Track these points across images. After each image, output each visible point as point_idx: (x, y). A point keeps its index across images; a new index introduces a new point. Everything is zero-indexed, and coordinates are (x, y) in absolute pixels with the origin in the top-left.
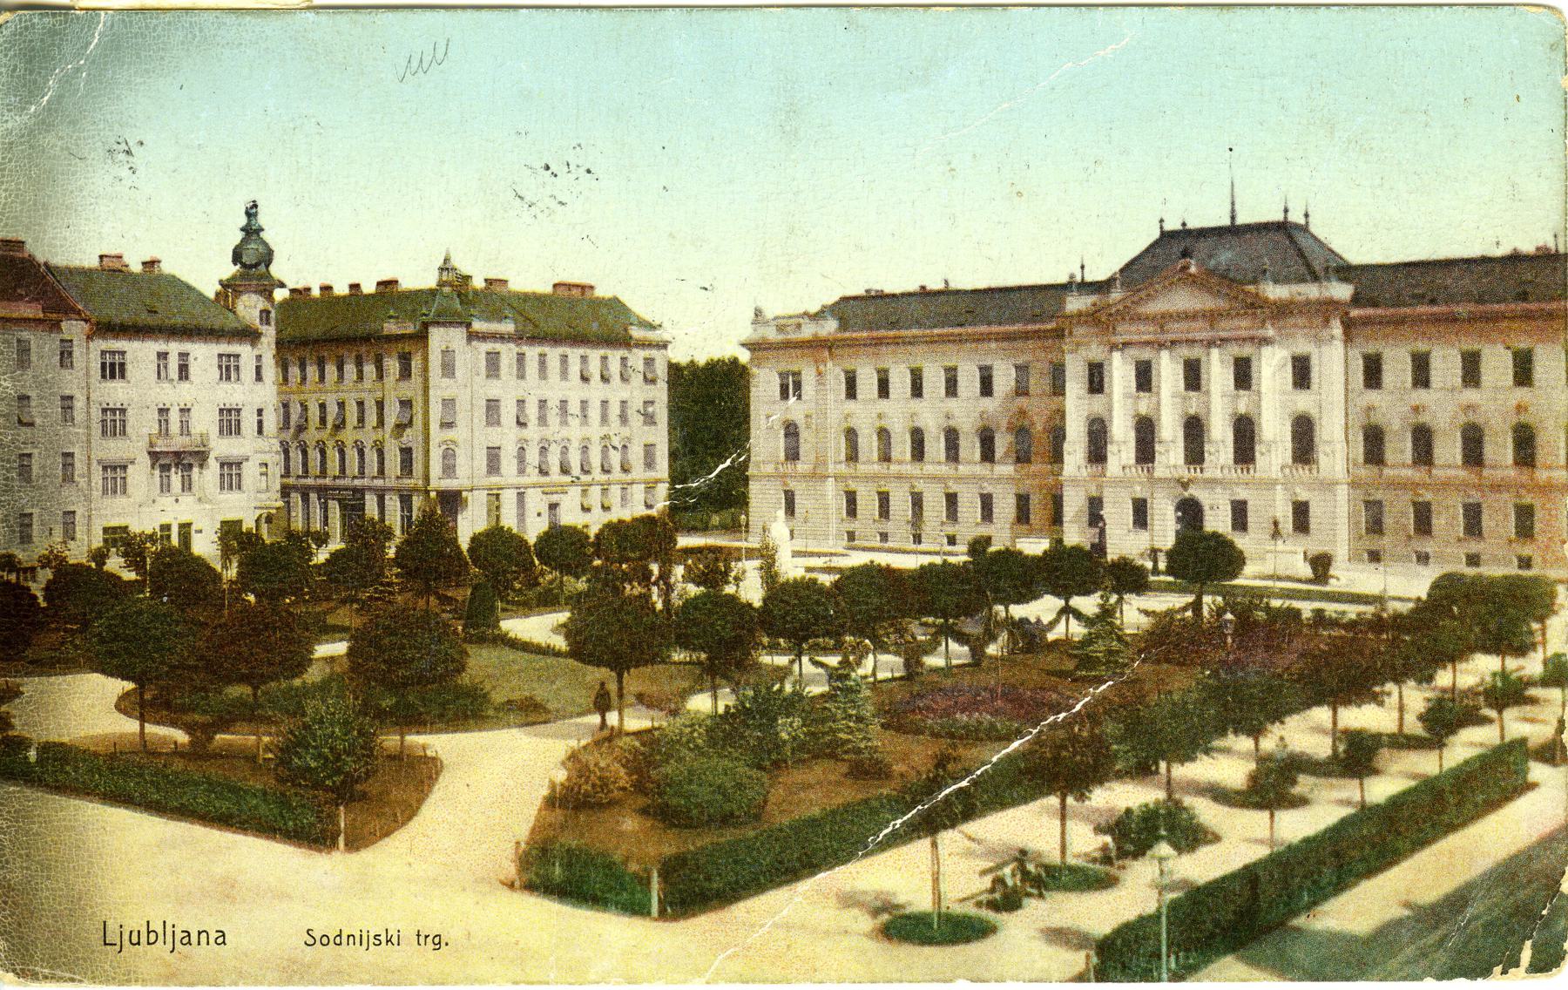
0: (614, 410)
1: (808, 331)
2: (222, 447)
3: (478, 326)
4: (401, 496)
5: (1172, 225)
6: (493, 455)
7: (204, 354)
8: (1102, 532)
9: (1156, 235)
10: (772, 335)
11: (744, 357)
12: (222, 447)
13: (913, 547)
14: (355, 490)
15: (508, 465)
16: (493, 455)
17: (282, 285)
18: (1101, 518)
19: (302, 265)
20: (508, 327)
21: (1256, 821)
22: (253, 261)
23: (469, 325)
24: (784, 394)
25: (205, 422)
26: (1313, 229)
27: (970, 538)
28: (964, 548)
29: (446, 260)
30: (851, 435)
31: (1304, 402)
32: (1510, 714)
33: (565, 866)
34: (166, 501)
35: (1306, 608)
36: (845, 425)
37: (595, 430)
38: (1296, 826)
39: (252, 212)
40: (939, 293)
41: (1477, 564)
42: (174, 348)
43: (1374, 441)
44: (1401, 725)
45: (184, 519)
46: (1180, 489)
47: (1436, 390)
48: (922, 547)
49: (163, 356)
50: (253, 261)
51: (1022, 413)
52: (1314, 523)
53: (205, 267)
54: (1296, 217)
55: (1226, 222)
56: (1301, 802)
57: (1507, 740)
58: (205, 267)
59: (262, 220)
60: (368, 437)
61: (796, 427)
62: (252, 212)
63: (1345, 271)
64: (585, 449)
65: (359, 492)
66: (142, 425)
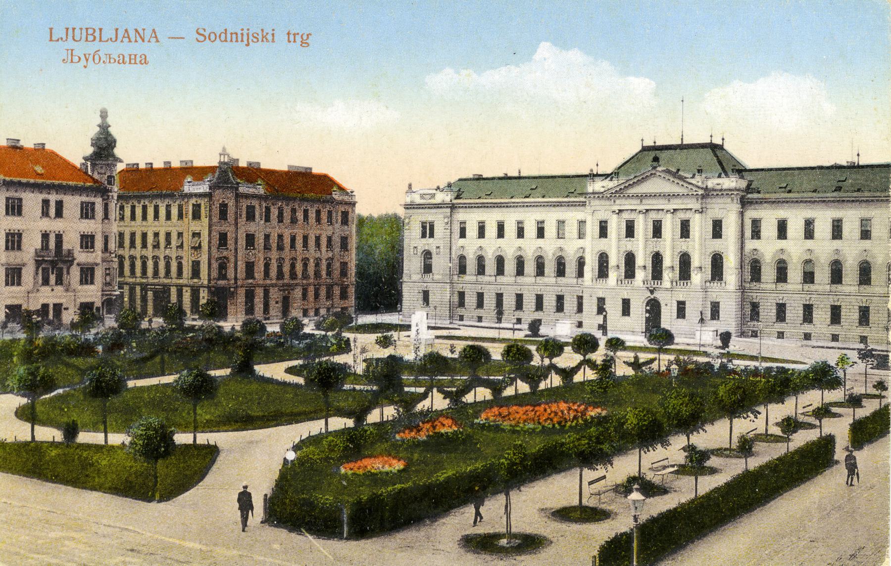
0: (324, 242)
1: (440, 197)
2: (82, 257)
3: (243, 189)
4: (192, 290)
5: (649, 143)
6: (250, 267)
7: (73, 203)
8: (605, 317)
9: (640, 148)
10: (418, 200)
11: (401, 212)
12: (82, 257)
13: (497, 325)
14: (164, 285)
15: (259, 273)
16: (250, 267)
17: (121, 161)
18: (604, 310)
19: (132, 152)
20: (261, 190)
21: (687, 481)
22: (104, 148)
23: (237, 189)
24: (424, 235)
25: (71, 242)
26: (725, 147)
27: (529, 321)
28: (526, 326)
29: (224, 149)
30: (462, 258)
31: (717, 245)
32: (825, 421)
33: (296, 506)
34: (47, 289)
35: (717, 363)
36: (519, 253)
37: (325, 254)
38: (707, 484)
39: (104, 115)
40: (515, 178)
41: (837, 340)
42: (53, 198)
43: (755, 269)
44: (731, 422)
45: (57, 301)
46: (649, 294)
47: (549, 239)
48: (502, 325)
49: (46, 202)
50: (104, 148)
51: (561, 249)
52: (421, 296)
53: (76, 150)
54: (717, 141)
55: (680, 143)
56: (713, 471)
57: (823, 435)
58: (76, 150)
59: (109, 120)
60: (161, 253)
61: (607, 256)
62: (104, 115)
63: (741, 171)
64: (317, 265)
65: (166, 289)
66: (32, 243)
